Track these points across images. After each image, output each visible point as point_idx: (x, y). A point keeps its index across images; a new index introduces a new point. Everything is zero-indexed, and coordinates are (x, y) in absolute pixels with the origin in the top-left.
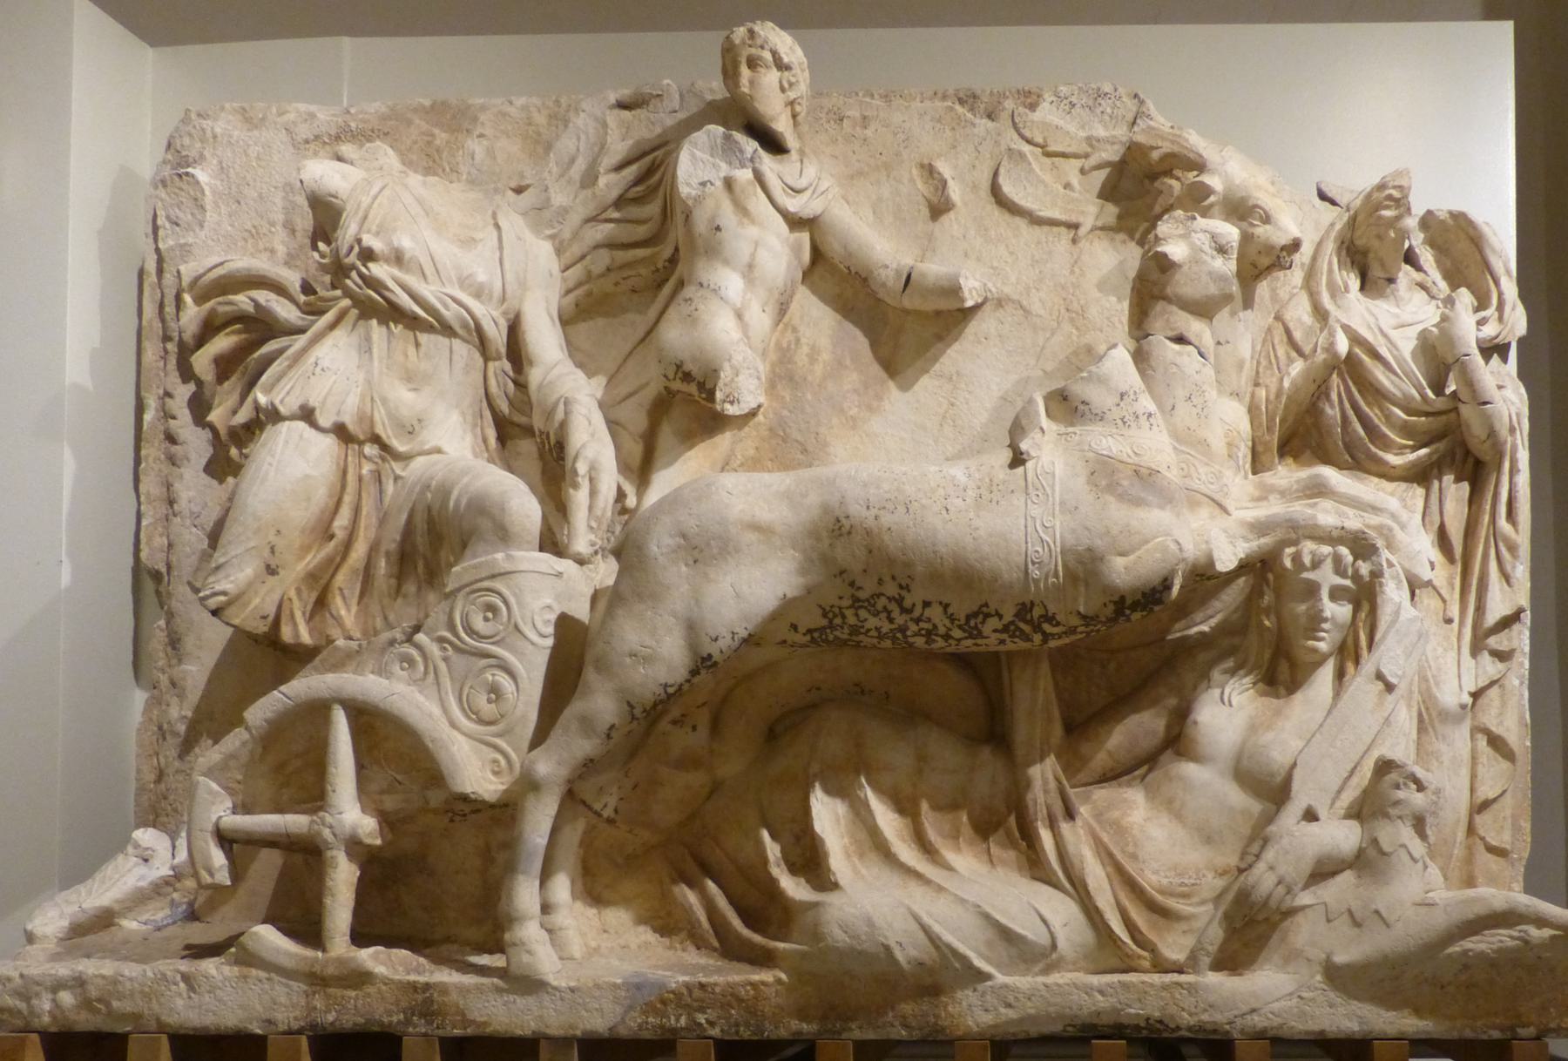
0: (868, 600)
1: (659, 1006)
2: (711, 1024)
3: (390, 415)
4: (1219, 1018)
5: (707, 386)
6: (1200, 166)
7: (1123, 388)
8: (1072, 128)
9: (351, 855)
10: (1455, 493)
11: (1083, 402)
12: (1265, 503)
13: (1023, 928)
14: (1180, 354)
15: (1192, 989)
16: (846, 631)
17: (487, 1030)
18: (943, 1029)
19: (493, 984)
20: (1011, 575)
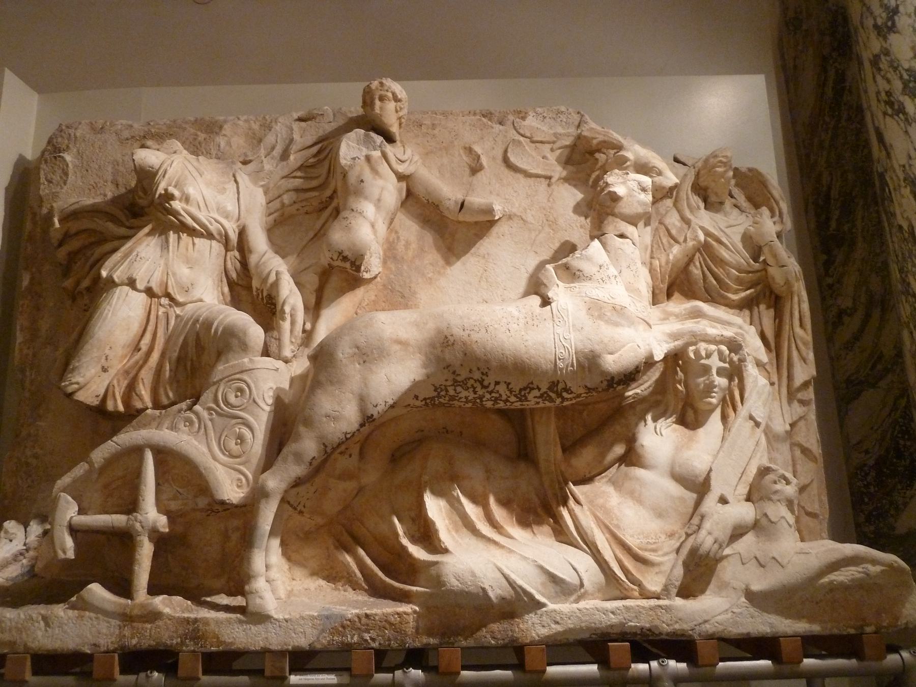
0: (463, 381)
1: (340, 629)
2: (373, 640)
3: (177, 282)
4: (685, 627)
5: (357, 264)
6: (620, 148)
7: (601, 263)
8: (545, 128)
9: (150, 539)
10: (767, 316)
11: (579, 270)
12: (667, 321)
13: (563, 574)
14: (623, 243)
15: (667, 609)
16: (447, 398)
17: (233, 648)
18: (517, 639)
19: (237, 618)
20: (547, 366)
